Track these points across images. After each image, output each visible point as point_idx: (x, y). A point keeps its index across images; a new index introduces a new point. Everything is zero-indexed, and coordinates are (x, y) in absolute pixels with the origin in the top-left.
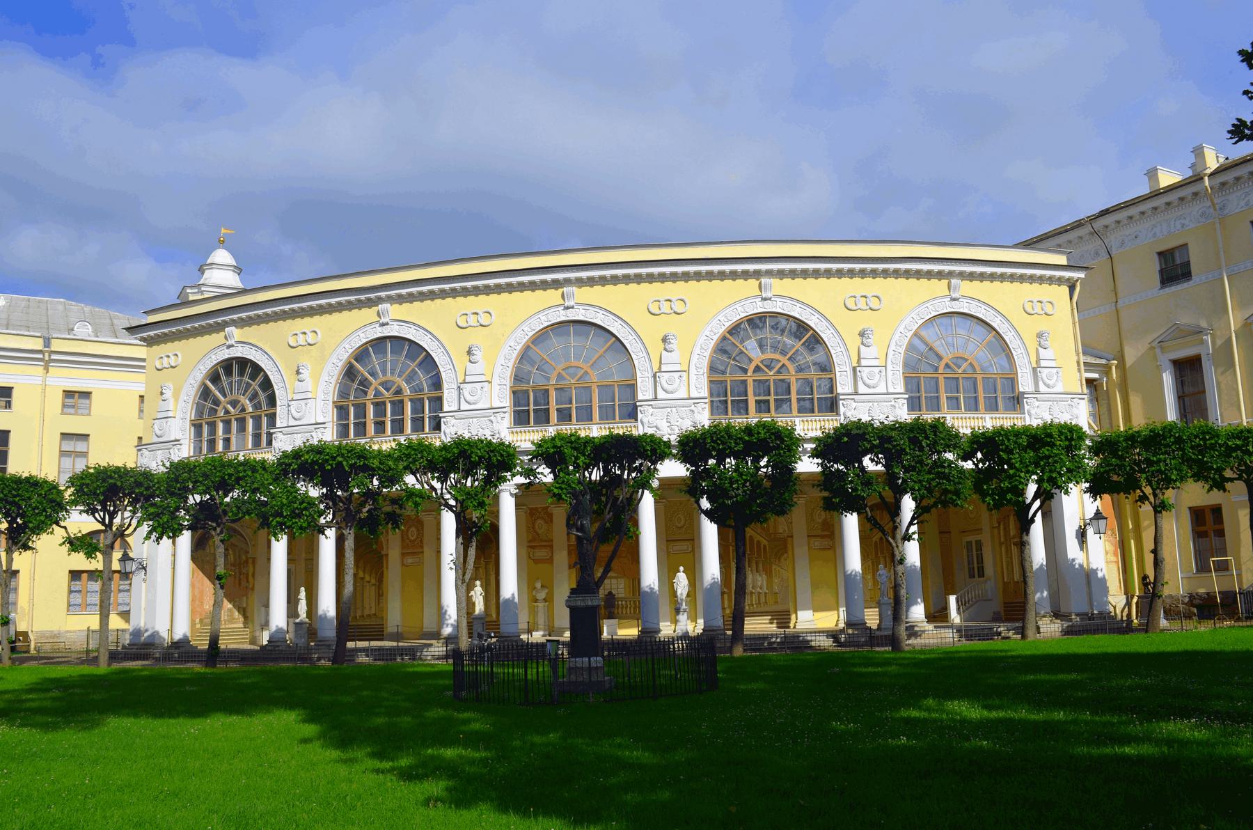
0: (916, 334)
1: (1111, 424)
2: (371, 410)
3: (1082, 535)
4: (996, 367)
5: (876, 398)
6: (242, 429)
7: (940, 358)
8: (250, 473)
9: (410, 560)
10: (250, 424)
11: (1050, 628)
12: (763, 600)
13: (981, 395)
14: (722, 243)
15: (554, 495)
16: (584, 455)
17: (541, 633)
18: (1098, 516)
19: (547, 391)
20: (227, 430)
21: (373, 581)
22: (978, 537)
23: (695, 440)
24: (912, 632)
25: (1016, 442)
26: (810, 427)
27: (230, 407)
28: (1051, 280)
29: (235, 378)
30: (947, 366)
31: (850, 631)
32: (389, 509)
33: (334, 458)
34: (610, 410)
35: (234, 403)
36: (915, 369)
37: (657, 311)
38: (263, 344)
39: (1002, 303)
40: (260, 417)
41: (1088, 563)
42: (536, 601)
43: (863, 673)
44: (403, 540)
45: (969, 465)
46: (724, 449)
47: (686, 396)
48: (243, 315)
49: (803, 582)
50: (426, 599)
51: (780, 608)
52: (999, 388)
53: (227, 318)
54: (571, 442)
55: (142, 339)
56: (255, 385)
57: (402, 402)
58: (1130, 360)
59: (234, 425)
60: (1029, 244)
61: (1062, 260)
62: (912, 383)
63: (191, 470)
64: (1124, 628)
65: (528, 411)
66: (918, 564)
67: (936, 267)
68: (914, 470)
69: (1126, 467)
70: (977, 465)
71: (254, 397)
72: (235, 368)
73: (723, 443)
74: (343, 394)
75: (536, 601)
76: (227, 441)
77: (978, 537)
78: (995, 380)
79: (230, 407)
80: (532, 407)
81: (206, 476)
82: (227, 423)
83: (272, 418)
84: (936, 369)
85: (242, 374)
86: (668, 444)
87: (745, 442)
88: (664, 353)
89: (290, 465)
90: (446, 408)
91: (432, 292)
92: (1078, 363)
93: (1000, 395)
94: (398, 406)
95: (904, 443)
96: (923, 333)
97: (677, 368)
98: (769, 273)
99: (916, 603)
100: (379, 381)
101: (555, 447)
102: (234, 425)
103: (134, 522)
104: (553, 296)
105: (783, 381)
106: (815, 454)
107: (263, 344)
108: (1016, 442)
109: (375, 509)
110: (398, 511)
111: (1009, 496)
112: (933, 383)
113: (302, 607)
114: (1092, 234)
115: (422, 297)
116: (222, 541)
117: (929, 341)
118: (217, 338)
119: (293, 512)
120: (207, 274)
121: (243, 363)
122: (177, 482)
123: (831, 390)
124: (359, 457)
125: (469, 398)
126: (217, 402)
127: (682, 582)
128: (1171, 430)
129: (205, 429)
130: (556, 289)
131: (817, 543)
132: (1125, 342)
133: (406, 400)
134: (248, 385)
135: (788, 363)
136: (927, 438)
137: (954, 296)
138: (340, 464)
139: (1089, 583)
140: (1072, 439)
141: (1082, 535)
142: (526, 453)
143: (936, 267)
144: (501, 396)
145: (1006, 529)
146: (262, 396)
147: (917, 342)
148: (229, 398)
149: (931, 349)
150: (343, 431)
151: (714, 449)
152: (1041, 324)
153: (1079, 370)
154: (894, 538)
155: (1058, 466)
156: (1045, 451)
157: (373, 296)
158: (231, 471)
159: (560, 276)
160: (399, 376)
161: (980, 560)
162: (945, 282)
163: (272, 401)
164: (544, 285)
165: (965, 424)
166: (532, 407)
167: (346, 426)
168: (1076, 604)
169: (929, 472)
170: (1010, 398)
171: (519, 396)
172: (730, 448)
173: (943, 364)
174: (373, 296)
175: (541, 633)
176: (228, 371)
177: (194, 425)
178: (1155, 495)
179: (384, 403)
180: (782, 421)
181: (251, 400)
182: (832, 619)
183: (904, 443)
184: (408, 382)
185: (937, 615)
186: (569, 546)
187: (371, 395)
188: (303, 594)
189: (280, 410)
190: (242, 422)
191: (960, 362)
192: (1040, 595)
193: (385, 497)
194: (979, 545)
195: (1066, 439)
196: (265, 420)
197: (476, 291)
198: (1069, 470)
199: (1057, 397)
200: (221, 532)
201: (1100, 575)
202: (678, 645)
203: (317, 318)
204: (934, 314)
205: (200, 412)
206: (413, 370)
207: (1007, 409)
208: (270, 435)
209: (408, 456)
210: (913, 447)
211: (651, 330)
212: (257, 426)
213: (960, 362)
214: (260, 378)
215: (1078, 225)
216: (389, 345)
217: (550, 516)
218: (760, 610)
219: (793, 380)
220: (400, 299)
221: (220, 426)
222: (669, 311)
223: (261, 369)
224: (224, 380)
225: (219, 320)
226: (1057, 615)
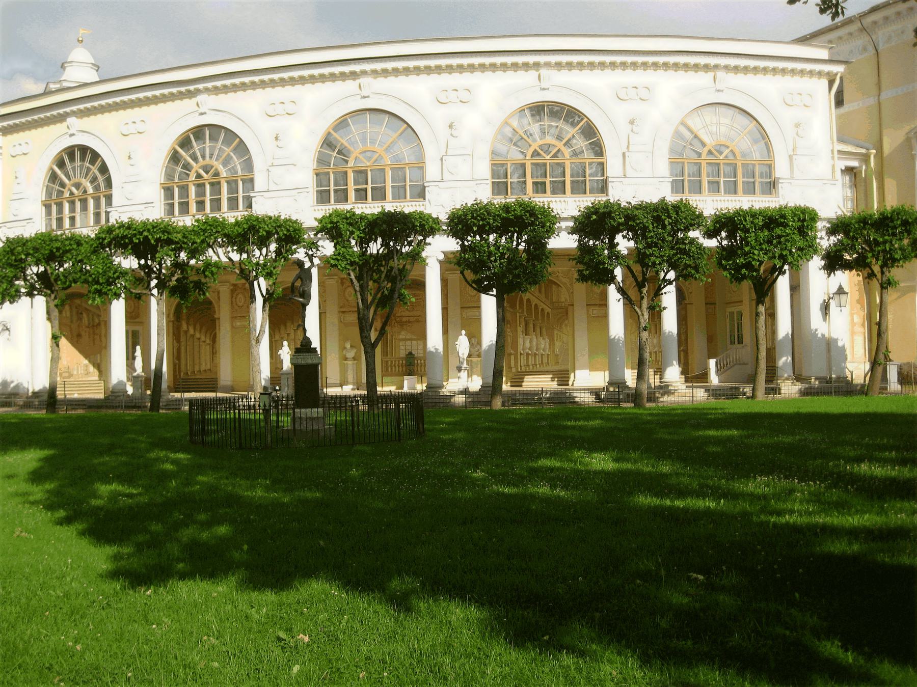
0: (683, 123)
1: (866, 205)
2: (192, 190)
3: (825, 308)
4: (757, 153)
5: (639, 180)
6: (85, 208)
7: (704, 145)
8: (75, 246)
10: (91, 203)
11: (789, 389)
12: (545, 360)
13: (740, 180)
14: (504, 36)
15: (333, 266)
16: (359, 230)
17: (351, 387)
18: (840, 291)
19: (346, 173)
20: (72, 210)
21: (208, 341)
22: (739, 308)
23: (459, 217)
24: (665, 389)
25: (752, 222)
26: (568, 206)
27: (74, 190)
28: (811, 73)
29: (78, 163)
30: (710, 152)
31: (612, 389)
32: (196, 278)
33: (141, 233)
34: (402, 191)
35: (78, 186)
36: (681, 154)
38: (101, 132)
39: (764, 92)
40: (99, 197)
41: (829, 333)
42: (346, 359)
43: (629, 423)
44: (232, 307)
45: (712, 243)
46: (484, 226)
48: (82, 107)
49: (582, 343)
51: (563, 368)
52: (757, 174)
53: (68, 110)
54: (347, 219)
56: (95, 170)
57: (219, 183)
58: (887, 149)
59: (78, 204)
60: (803, 40)
61: (824, 54)
62: (677, 166)
63: (24, 244)
64: (863, 391)
65: (329, 191)
66: (675, 331)
67: (702, 60)
68: (656, 246)
69: (873, 244)
70: (720, 244)
71: (94, 180)
72: (78, 154)
73: (483, 220)
74: (169, 176)
75: (346, 359)
76: (72, 219)
77: (739, 308)
78: (754, 165)
79: (74, 190)
80: (332, 187)
81: (36, 249)
82: (72, 203)
83: (109, 198)
84: (700, 155)
85: (83, 159)
86: (437, 221)
87: (503, 219)
89: (104, 239)
91: (234, 85)
93: (758, 180)
94: (216, 186)
95: (648, 222)
96: (690, 123)
98: (548, 65)
99: (672, 365)
100: (199, 165)
101: (331, 222)
102: (78, 204)
104: (350, 86)
105: (558, 164)
106: (573, 231)
107: (101, 132)
108: (752, 222)
109: (184, 278)
110: (203, 280)
111: (744, 271)
112: (696, 168)
113: (139, 363)
115: (235, 88)
116: (56, 306)
117: (695, 129)
118: (59, 128)
119: (108, 281)
120: (69, 70)
121: (84, 149)
122: (13, 254)
123: (770, 174)
124: (163, 232)
126: (63, 185)
127: (463, 345)
128: (898, 214)
129: (54, 208)
130: (354, 79)
132: (885, 132)
135: (563, 149)
136: (670, 217)
138: (146, 237)
139: (829, 350)
140: (804, 220)
141: (825, 308)
142: (312, 229)
143: (702, 60)
144: (305, 177)
146: (101, 179)
147: (683, 130)
149: (696, 136)
150: (170, 210)
151: (475, 225)
153: (833, 158)
154: (640, 307)
155: (789, 244)
156: (778, 231)
157: (192, 88)
158: (58, 244)
159: (357, 68)
160: (217, 160)
161: (740, 328)
162: (710, 75)
163: (109, 183)
164: (343, 76)
165: (709, 205)
166: (332, 187)
167: (172, 205)
168: (816, 370)
169: (672, 248)
170: (767, 183)
171: (321, 177)
172: (489, 224)
173: (706, 150)
174: (192, 88)
175: (351, 387)
177: (45, 205)
178: (883, 273)
179: (204, 185)
180: (540, 200)
182: (599, 379)
183: (648, 222)
184: (225, 165)
185: (694, 376)
187: (193, 177)
189: (116, 192)
190: (84, 202)
191: (722, 149)
192: (784, 360)
193: (192, 267)
194: (740, 315)
195: (799, 220)
196: (103, 201)
197: (283, 82)
198: (800, 249)
199: (817, 182)
200: (55, 298)
201: (840, 344)
202: (460, 399)
203: (145, 108)
205: (49, 193)
206: (229, 155)
207: (763, 193)
208: (107, 213)
209: (204, 231)
210: (660, 228)
212: (97, 205)
213: (722, 149)
216: (223, 135)
218: (542, 369)
220: (216, 90)
221: (66, 206)
225: (61, 111)
226: (798, 378)
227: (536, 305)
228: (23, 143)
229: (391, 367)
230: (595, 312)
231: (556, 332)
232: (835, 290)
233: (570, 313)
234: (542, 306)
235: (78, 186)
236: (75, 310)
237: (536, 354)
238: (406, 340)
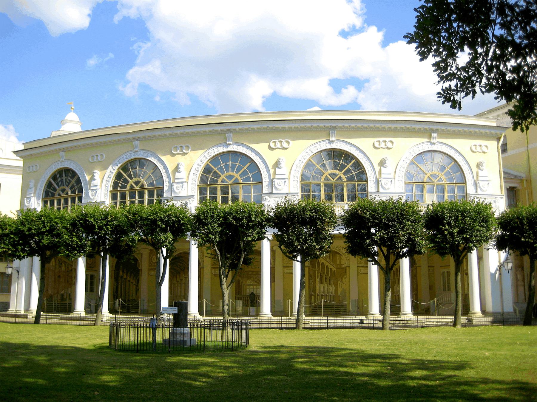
21: (134, 283)
27: (61, 193)
29: (64, 178)
35: (63, 191)
37: (378, 146)
39: (462, 148)
55: (20, 157)
56: (73, 182)
60: (481, 115)
85: (67, 176)
88: (479, 171)
126: (55, 190)
148: (61, 188)
176: (61, 176)
211: (376, 156)
214: (76, 178)
219: (345, 184)
222: (384, 147)
224: (59, 179)
231: (339, 282)
233: (347, 271)
236: (57, 261)
237: (326, 296)
238: (250, 285)
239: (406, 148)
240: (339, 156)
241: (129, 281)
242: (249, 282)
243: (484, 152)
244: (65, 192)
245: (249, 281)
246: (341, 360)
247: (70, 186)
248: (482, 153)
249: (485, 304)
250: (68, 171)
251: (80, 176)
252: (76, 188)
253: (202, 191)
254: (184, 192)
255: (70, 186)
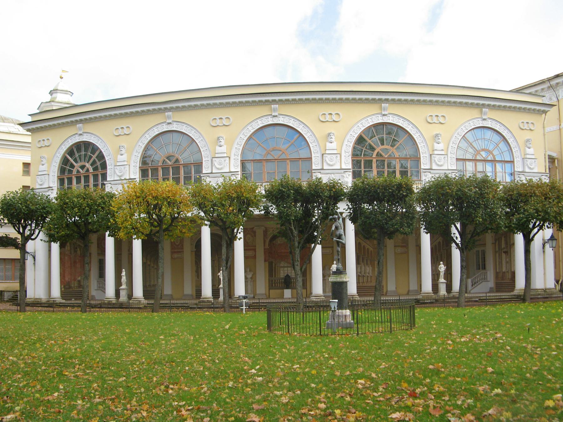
9: (176, 256)
40: (64, 179)
47: (339, 168)
50: (411, 276)
55: (28, 130)
57: (89, 176)
83: (104, 177)
85: (86, 150)
90: (204, 171)
92: (545, 155)
96: (469, 136)
97: (335, 152)
103: (37, 231)
114: (549, 87)
125: (218, 166)
126: (72, 166)
131: (399, 250)
133: (73, 177)
134: (80, 156)
137: (484, 117)
145: (500, 245)
148: (80, 164)
152: (527, 135)
176: (79, 150)
181: (92, 165)
186: (265, 249)
188: (124, 273)
194: (484, 253)
204: (473, 127)
208: (103, 184)
215: (542, 82)
217: (255, 232)
223: (98, 148)
224: (77, 155)
227: (364, 246)
228: (224, 118)
229: (275, 284)
230: (399, 250)
232: (549, 238)
234: (367, 247)
235: (83, 167)
237: (364, 276)
238: (284, 267)
239: (462, 121)
240: (389, 132)
241: (149, 265)
242: (282, 264)
243: (530, 130)
244: (85, 169)
245: (282, 263)
246: (148, 304)
247: (91, 161)
248: (529, 131)
249: (417, 274)
250: (87, 145)
251: (103, 151)
252: (98, 163)
253: (61, 181)
254: (333, 163)
255: (91, 161)
